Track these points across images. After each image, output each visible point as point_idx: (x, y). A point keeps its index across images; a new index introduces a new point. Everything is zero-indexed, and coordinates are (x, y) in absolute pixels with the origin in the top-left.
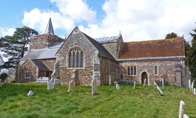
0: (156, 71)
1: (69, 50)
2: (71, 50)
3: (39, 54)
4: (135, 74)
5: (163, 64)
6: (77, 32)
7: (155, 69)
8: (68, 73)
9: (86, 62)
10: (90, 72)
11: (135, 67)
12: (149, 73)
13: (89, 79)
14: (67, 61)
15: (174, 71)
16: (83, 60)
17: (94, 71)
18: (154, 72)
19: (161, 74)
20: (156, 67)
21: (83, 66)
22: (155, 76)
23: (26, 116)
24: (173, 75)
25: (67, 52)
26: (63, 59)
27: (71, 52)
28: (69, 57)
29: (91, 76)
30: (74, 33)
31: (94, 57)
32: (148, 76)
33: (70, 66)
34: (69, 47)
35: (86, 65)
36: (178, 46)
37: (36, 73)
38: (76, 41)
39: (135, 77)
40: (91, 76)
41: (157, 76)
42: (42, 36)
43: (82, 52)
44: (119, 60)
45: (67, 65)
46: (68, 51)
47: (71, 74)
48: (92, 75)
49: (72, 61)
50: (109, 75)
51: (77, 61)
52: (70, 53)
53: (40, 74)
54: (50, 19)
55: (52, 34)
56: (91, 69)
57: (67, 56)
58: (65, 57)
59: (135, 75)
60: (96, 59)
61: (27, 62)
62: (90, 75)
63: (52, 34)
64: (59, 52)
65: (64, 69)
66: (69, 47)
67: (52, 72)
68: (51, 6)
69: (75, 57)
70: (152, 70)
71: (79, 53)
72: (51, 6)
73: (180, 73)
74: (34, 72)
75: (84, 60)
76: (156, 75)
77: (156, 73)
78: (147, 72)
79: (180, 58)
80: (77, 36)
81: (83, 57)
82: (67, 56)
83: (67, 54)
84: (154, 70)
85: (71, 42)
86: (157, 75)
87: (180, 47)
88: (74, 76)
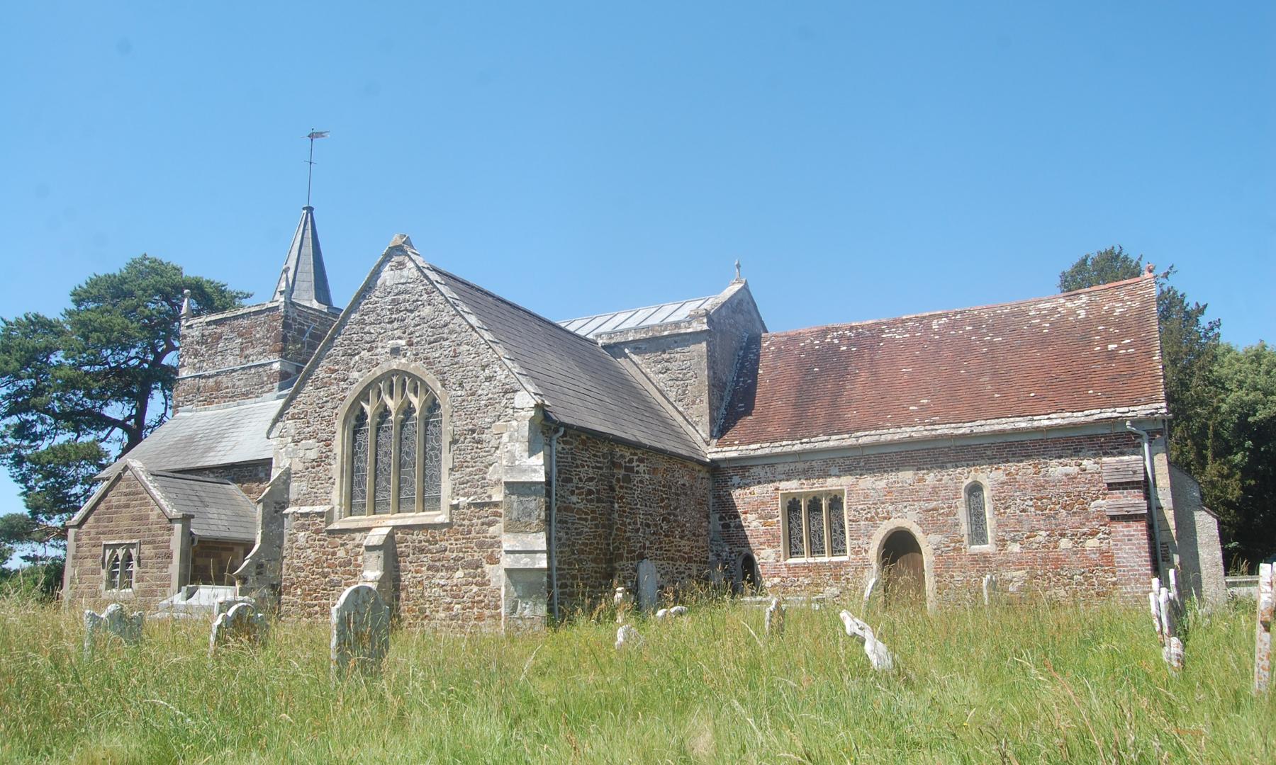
0: (977, 516)
1: (351, 395)
2: (364, 395)
3: (222, 436)
4: (838, 548)
5: (1024, 469)
6: (405, 272)
8: (341, 553)
9: (458, 475)
10: (481, 545)
12: (935, 538)
13: (475, 589)
15: (1100, 516)
16: (439, 461)
18: (964, 528)
19: (1014, 540)
20: (975, 489)
21: (438, 500)
24: (1092, 543)
26: (313, 455)
27: (368, 409)
28: (355, 440)
29: (487, 567)
30: (387, 276)
32: (928, 557)
33: (358, 500)
35: (455, 493)
36: (1117, 339)
37: (169, 556)
38: (398, 333)
39: (839, 565)
40: (487, 567)
41: (985, 558)
42: (245, 322)
43: (432, 407)
44: (729, 455)
46: (348, 402)
48: (493, 560)
49: (369, 468)
50: (641, 557)
52: (362, 417)
53: (200, 561)
54: (310, 209)
55: (315, 305)
57: (338, 436)
58: (328, 442)
59: (834, 552)
60: (520, 448)
61: (122, 486)
62: (479, 566)
63: (315, 305)
64: (291, 410)
65: (319, 523)
66: (355, 375)
67: (253, 545)
68: (320, 135)
69: (392, 444)
72: (320, 135)
73: (1138, 531)
76: (976, 548)
77: (978, 535)
78: (917, 531)
79: (1133, 423)
80: (401, 297)
81: (438, 439)
82: (338, 436)
83: (338, 426)
84: (962, 515)
85: (367, 338)
86: (988, 548)
87: (1127, 347)
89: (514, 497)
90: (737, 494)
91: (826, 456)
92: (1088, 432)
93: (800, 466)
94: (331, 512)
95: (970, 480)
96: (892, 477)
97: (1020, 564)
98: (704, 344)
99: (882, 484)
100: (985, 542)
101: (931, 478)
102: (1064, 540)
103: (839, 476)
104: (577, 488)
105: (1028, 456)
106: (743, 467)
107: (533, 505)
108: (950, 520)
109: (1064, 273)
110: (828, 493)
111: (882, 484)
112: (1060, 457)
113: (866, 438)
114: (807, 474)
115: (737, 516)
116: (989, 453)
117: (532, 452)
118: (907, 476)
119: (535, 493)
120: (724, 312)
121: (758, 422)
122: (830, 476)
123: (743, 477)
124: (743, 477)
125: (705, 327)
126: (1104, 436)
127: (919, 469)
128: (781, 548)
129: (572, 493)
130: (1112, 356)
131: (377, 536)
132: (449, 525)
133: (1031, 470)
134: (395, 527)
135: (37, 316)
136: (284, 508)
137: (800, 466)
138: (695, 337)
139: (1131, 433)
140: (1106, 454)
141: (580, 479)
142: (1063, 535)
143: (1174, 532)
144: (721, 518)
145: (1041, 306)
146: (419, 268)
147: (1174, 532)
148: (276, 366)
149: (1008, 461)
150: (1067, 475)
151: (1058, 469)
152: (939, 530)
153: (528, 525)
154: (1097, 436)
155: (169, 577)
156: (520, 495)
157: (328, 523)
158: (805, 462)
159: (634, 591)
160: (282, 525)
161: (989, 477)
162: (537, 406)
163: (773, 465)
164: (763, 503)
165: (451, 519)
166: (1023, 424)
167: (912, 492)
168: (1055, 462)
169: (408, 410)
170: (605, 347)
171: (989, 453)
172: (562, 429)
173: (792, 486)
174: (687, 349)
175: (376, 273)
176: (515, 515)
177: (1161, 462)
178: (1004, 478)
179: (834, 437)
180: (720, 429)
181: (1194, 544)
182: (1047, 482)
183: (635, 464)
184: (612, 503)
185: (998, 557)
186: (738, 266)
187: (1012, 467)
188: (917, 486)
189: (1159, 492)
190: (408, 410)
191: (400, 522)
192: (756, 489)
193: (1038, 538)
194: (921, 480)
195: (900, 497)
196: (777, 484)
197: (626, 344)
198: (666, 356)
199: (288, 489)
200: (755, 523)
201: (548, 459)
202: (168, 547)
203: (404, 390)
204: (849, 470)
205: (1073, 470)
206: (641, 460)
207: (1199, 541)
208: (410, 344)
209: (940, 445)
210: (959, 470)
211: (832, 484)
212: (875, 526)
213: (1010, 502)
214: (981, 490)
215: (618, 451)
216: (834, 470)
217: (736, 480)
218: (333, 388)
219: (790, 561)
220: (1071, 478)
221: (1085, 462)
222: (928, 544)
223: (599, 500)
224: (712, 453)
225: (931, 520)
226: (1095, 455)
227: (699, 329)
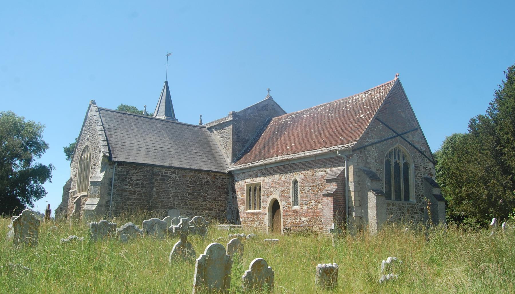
0: (295, 193)
5: (308, 173)
18: (291, 199)
20: (295, 182)
30: (89, 115)
39: (259, 213)
54: (167, 83)
60: (99, 170)
90: (236, 184)
92: (328, 157)
93: (251, 173)
97: (306, 215)
98: (232, 125)
99: (271, 180)
102: (320, 205)
105: (311, 168)
107: (97, 189)
109: (47, 148)
113: (272, 160)
114: (253, 176)
115: (236, 193)
117: (102, 171)
118: (277, 176)
119: (98, 185)
120: (249, 111)
121: (249, 155)
125: (232, 119)
126: (334, 158)
129: (126, 185)
130: (360, 118)
137: (251, 173)
140: (334, 166)
141: (132, 180)
143: (353, 202)
144: (232, 194)
147: (353, 202)
150: (321, 176)
151: (320, 173)
152: (285, 200)
153: (95, 196)
156: (94, 186)
157: (74, 195)
159: (137, 217)
160: (68, 196)
161: (299, 176)
163: (244, 173)
164: (242, 188)
166: (308, 153)
168: (318, 170)
170: (208, 129)
172: (117, 163)
173: (248, 181)
177: (351, 168)
178: (303, 177)
182: (315, 179)
183: (169, 174)
185: (300, 211)
187: (306, 172)
188: (280, 181)
189: (350, 184)
191: (82, 195)
192: (240, 182)
193: (312, 204)
194: (281, 178)
195: (275, 185)
197: (213, 127)
198: (223, 131)
201: (105, 175)
204: (263, 174)
205: (323, 173)
206: (172, 173)
209: (286, 163)
211: (259, 180)
215: (157, 170)
219: (248, 211)
220: (323, 177)
222: (282, 204)
223: (142, 187)
224: (230, 167)
226: (331, 167)
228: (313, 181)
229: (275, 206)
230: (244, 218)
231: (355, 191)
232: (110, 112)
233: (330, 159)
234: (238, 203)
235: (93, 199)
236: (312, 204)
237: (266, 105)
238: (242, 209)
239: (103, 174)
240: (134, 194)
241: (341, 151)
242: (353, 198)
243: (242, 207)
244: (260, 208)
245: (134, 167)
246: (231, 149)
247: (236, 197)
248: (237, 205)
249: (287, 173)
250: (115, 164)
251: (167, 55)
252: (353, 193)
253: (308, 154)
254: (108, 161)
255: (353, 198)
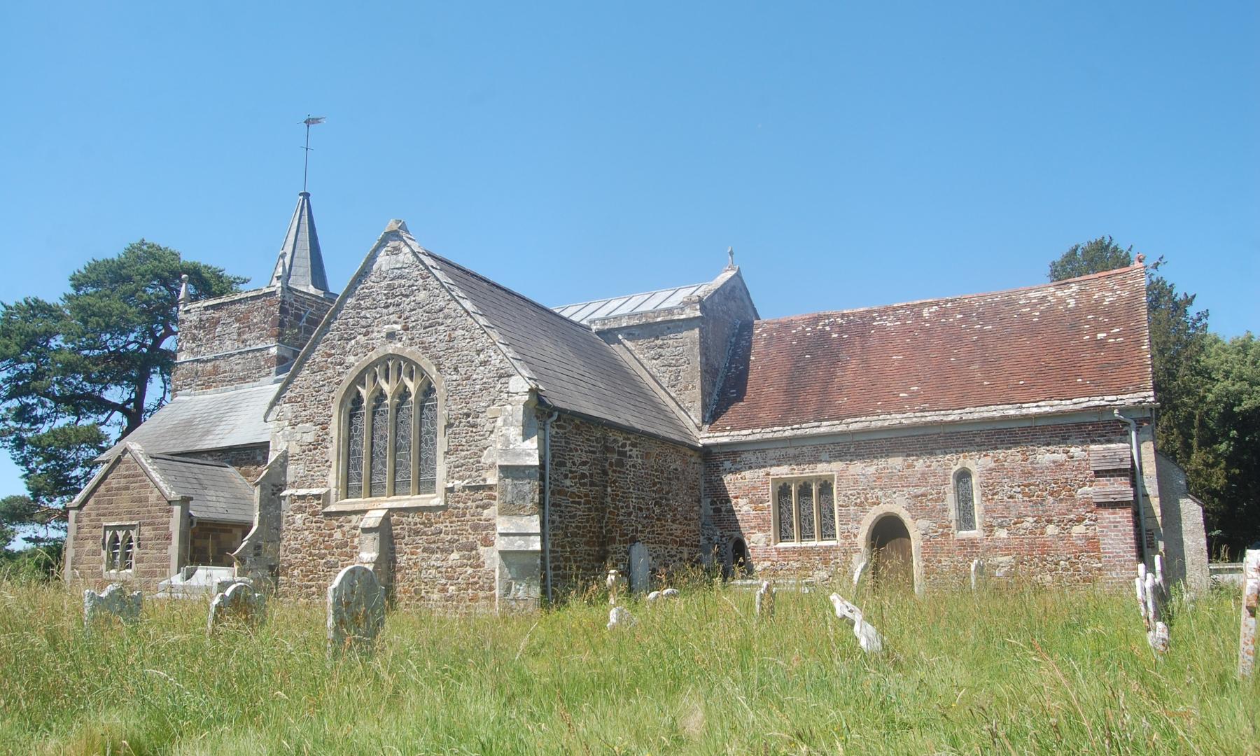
0: (965, 502)
1: (347, 379)
2: (360, 379)
4: (827, 532)
5: (1012, 456)
6: (401, 257)
7: (957, 488)
8: (338, 535)
9: (453, 458)
10: (475, 528)
11: (826, 487)
12: (924, 523)
13: (470, 571)
14: (332, 451)
15: (1086, 503)
16: (434, 444)
17: (502, 513)
18: (953, 514)
19: (1001, 526)
20: (963, 476)
21: (434, 483)
22: (963, 544)
23: (1228, 667)
24: (1078, 529)
25: (339, 393)
26: (310, 438)
27: (364, 393)
28: (351, 424)
29: (482, 549)
31: (500, 422)
32: (916, 541)
34: (351, 359)
35: (450, 476)
37: (168, 538)
39: (828, 550)
40: (482, 549)
41: (972, 543)
42: (243, 307)
43: (428, 391)
44: (720, 440)
45: (333, 479)
47: (356, 540)
48: (488, 543)
49: (365, 451)
50: (634, 540)
51: (396, 449)
52: (358, 400)
53: (198, 543)
55: (312, 290)
56: (485, 507)
57: (335, 420)
58: (324, 426)
59: (823, 536)
60: (515, 432)
62: (474, 548)
63: (312, 290)
64: (288, 394)
66: (351, 359)
68: (316, 121)
69: (388, 427)
70: (940, 499)
71: (388, 402)
72: (316, 121)
73: (1124, 518)
74: (157, 537)
75: (442, 443)
76: (964, 534)
77: (966, 521)
79: (1121, 411)
80: (397, 282)
82: (335, 420)
84: (951, 500)
85: (363, 322)
86: (976, 533)
87: (1116, 336)
88: (374, 555)
89: (508, 481)
90: (728, 479)
91: (816, 442)
92: (1077, 420)
93: (791, 452)
94: (328, 494)
95: (958, 467)
96: (882, 463)
97: (1007, 549)
98: (697, 331)
99: (872, 470)
100: (972, 528)
101: (920, 464)
103: (829, 462)
104: (571, 472)
105: (1017, 444)
106: (734, 453)
107: (527, 488)
108: (939, 506)
110: (818, 478)
111: (872, 470)
112: (1048, 445)
114: (797, 459)
115: (728, 501)
116: (978, 440)
118: (896, 462)
119: (529, 477)
122: (821, 461)
123: (734, 462)
124: (734, 462)
125: (698, 314)
126: (1092, 423)
127: (908, 455)
128: (771, 533)
129: (566, 476)
131: (373, 518)
132: (444, 508)
133: (1020, 457)
134: (390, 510)
135: (36, 301)
136: (281, 490)
137: (791, 452)
138: (688, 323)
139: (1119, 421)
140: (1093, 442)
142: (1049, 522)
143: (1159, 519)
145: (1031, 295)
146: (414, 253)
147: (1159, 519)
148: (274, 351)
149: (996, 448)
150: (1054, 462)
151: (1046, 456)
152: (928, 516)
154: (1085, 424)
155: (168, 558)
157: (325, 506)
158: (796, 448)
161: (978, 464)
162: (531, 390)
163: (764, 450)
164: (754, 488)
165: (446, 502)
167: (901, 477)
168: (1043, 449)
169: (403, 395)
170: (599, 333)
171: (978, 440)
172: (556, 414)
173: (783, 471)
174: (679, 336)
175: (372, 258)
176: (509, 498)
177: (1148, 450)
178: (993, 465)
179: (824, 423)
180: (713, 414)
181: (1179, 530)
182: (1035, 469)
183: (627, 448)
184: (605, 487)
185: (985, 543)
186: (731, 253)
187: (1001, 454)
190: (403, 395)
191: (395, 505)
194: (911, 466)
195: (889, 483)
196: (768, 469)
197: (620, 330)
198: (659, 342)
199: (285, 472)
200: (746, 508)
202: (168, 529)
203: (399, 374)
204: (839, 456)
205: (1061, 457)
207: (1184, 528)
208: (406, 329)
210: (948, 457)
211: (822, 469)
212: (864, 511)
213: (998, 488)
214: (970, 476)
216: (825, 456)
217: (727, 465)
218: (330, 372)
221: (1072, 449)
222: (916, 529)
223: (592, 484)
224: (704, 438)
225: (920, 505)
226: (1083, 443)
227: (692, 315)
228: (1027, 474)
229: (888, 533)
230: (767, 564)
231: (1161, 496)
232: (473, 279)
233: (1079, 425)
234: (741, 525)
235: (515, 519)
236: (1025, 525)
237: (733, 289)
238: (757, 541)
239: (532, 444)
240: (579, 503)
241: (1124, 410)
242: (1158, 511)
243: (760, 535)
244: (827, 532)
245: (577, 427)
246: (698, 391)
247: (731, 511)
248: (738, 529)
249: (931, 454)
250: (550, 415)
251: (308, 122)
252: (1158, 500)
253: (1012, 412)
254: (540, 412)
255: (1158, 511)
